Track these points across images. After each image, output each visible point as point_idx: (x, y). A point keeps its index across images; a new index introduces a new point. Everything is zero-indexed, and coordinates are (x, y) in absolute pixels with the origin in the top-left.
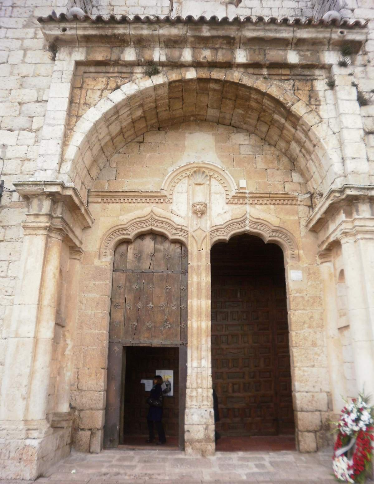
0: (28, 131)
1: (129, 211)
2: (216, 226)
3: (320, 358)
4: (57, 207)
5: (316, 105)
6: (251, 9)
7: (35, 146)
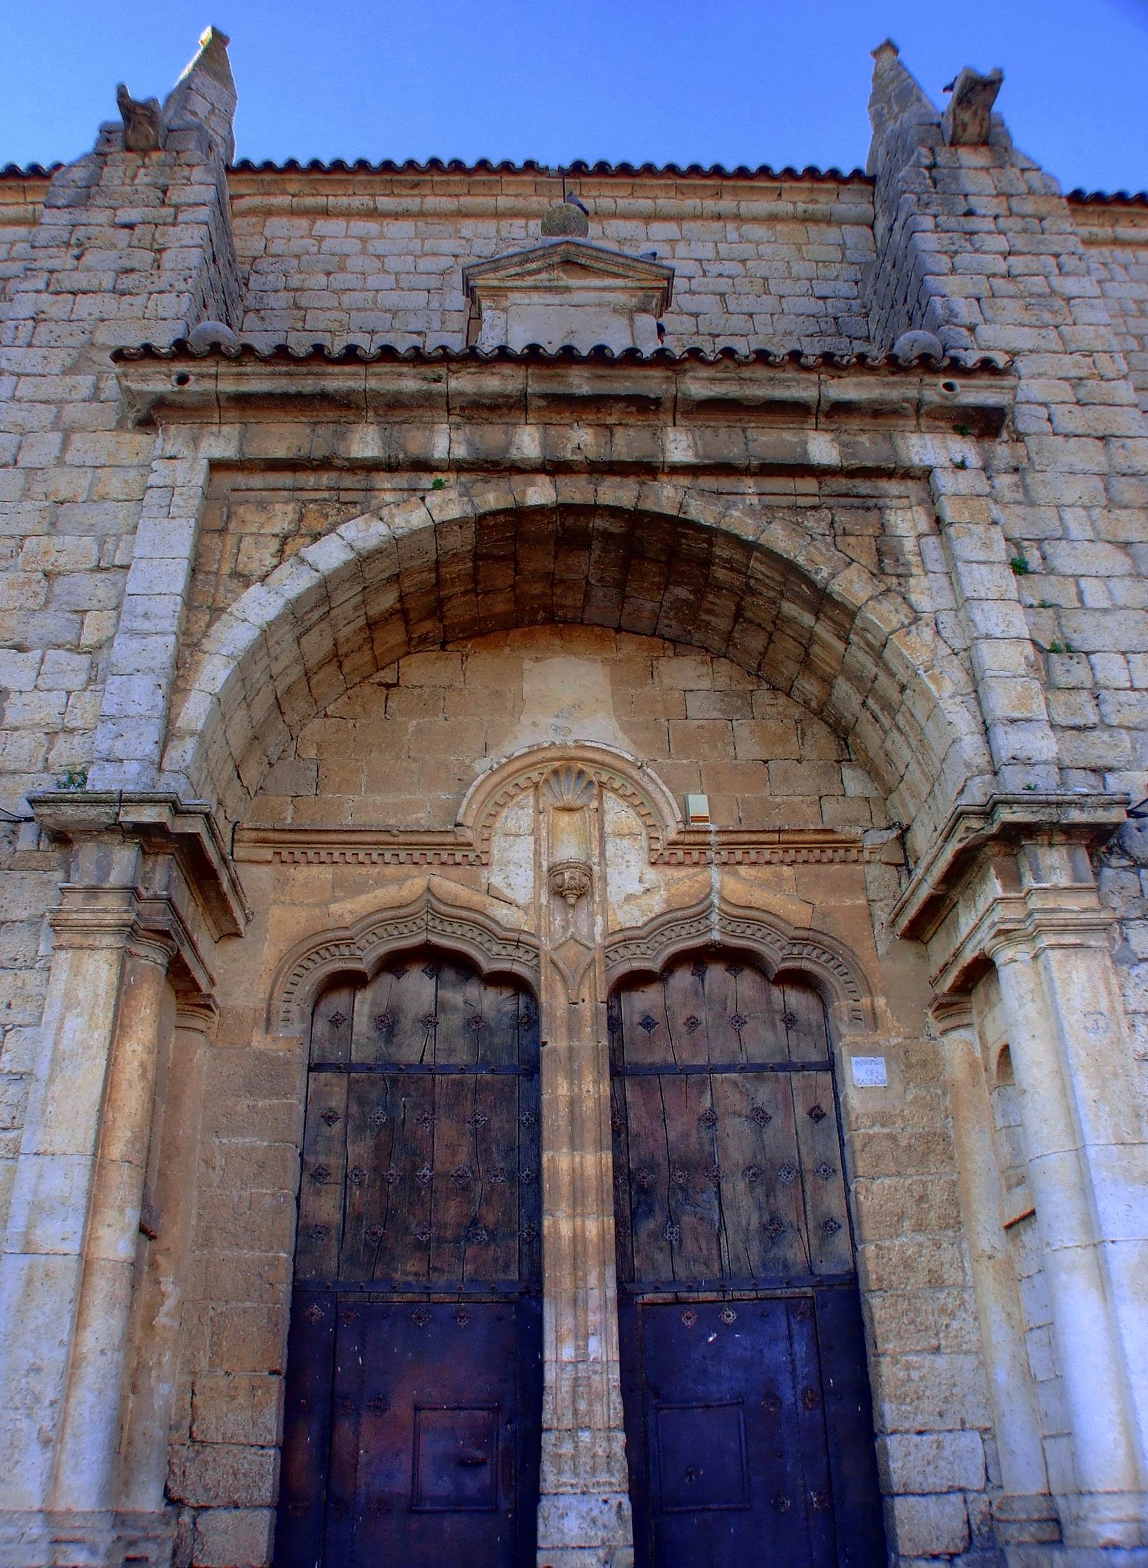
0: (70, 650)
1: (358, 888)
2: (621, 930)
3: (955, 1325)
4: (153, 870)
5: (898, 576)
6: (696, 315)
7: (88, 693)
